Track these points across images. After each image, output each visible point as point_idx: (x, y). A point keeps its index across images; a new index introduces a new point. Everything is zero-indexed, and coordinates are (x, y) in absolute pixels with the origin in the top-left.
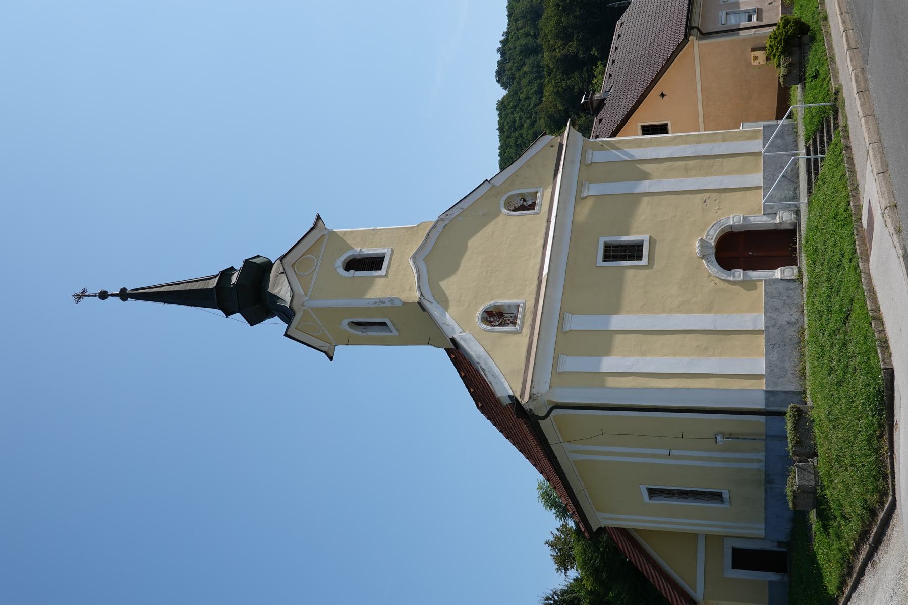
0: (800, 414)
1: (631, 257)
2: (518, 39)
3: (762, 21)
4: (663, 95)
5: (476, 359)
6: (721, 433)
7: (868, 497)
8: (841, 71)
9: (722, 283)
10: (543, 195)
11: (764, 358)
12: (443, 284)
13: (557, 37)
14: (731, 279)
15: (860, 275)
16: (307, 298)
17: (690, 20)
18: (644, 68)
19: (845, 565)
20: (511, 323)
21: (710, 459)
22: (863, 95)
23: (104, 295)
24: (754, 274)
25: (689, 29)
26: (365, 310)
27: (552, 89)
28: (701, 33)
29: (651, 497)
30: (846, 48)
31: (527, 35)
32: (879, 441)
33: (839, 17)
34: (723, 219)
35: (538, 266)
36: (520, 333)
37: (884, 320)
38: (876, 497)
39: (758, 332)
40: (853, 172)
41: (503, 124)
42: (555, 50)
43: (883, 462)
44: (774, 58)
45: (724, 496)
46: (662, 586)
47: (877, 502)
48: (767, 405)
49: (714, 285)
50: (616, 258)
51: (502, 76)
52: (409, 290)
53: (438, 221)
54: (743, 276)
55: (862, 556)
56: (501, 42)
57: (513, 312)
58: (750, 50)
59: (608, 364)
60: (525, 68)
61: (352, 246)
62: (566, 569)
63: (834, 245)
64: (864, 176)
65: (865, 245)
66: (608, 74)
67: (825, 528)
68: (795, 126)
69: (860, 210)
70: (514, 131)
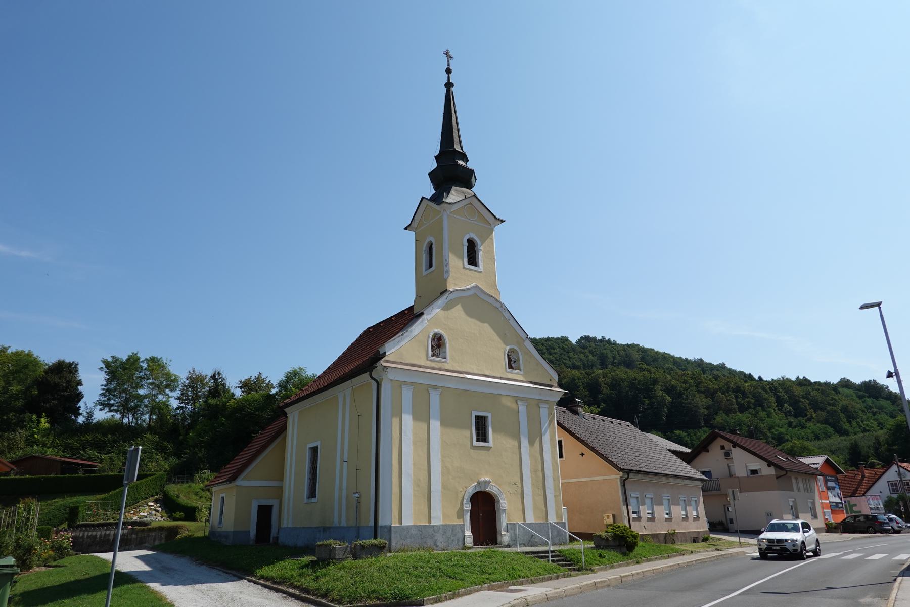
0: (381, 548)
1: (478, 435)
2: (612, 351)
3: (633, 521)
4: (583, 454)
5: (410, 330)
6: (360, 496)
7: (336, 592)
8: (605, 572)
9: (462, 496)
10: (518, 374)
11: (412, 524)
12: (459, 307)
13: (613, 379)
14: (465, 502)
15: (479, 584)
16: (449, 213)
17: (633, 473)
18: (601, 442)
19: (281, 580)
20: (434, 353)
21: (341, 489)
22: (593, 585)
23: (449, 71)
24: (467, 517)
25: (628, 472)
26: (441, 253)
27: (577, 375)
28: (625, 480)
29: (311, 448)
30: (622, 575)
31: (614, 358)
32: (375, 598)
33: (641, 571)
34: (504, 496)
35: (471, 371)
36: (427, 360)
37: (453, 600)
38: (337, 597)
39: (430, 520)
40: (542, 580)
41: (552, 341)
42: (604, 377)
43: (361, 601)
44: (612, 529)
45: (313, 498)
46: (243, 456)
47: (333, 598)
48: (381, 527)
50: (477, 424)
51: (586, 341)
52: (455, 284)
53: (500, 303)
55: (290, 591)
56: (609, 339)
57: (441, 354)
58: (614, 513)
59: (408, 419)
60: (591, 356)
61: (484, 244)
62: (241, 387)
63: (496, 568)
64: (542, 587)
65: (499, 588)
66: (595, 417)
67: (306, 566)
68: (565, 544)
69: (520, 585)
70: (547, 349)
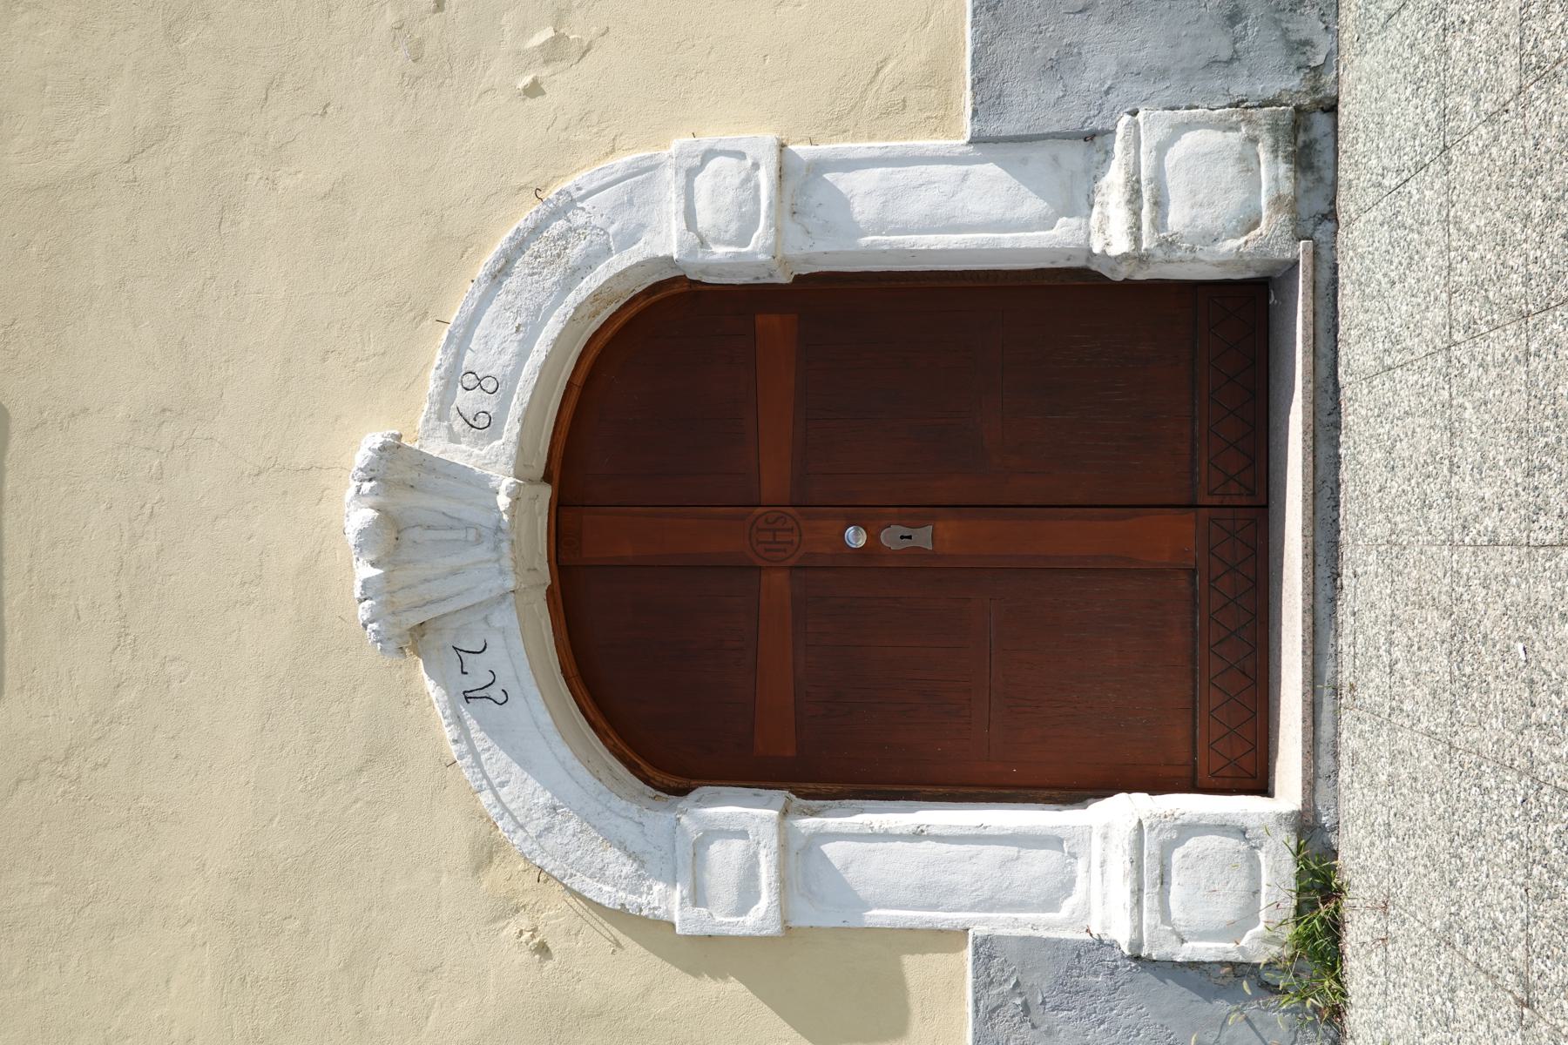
49: (524, 956)
54: (784, 884)
